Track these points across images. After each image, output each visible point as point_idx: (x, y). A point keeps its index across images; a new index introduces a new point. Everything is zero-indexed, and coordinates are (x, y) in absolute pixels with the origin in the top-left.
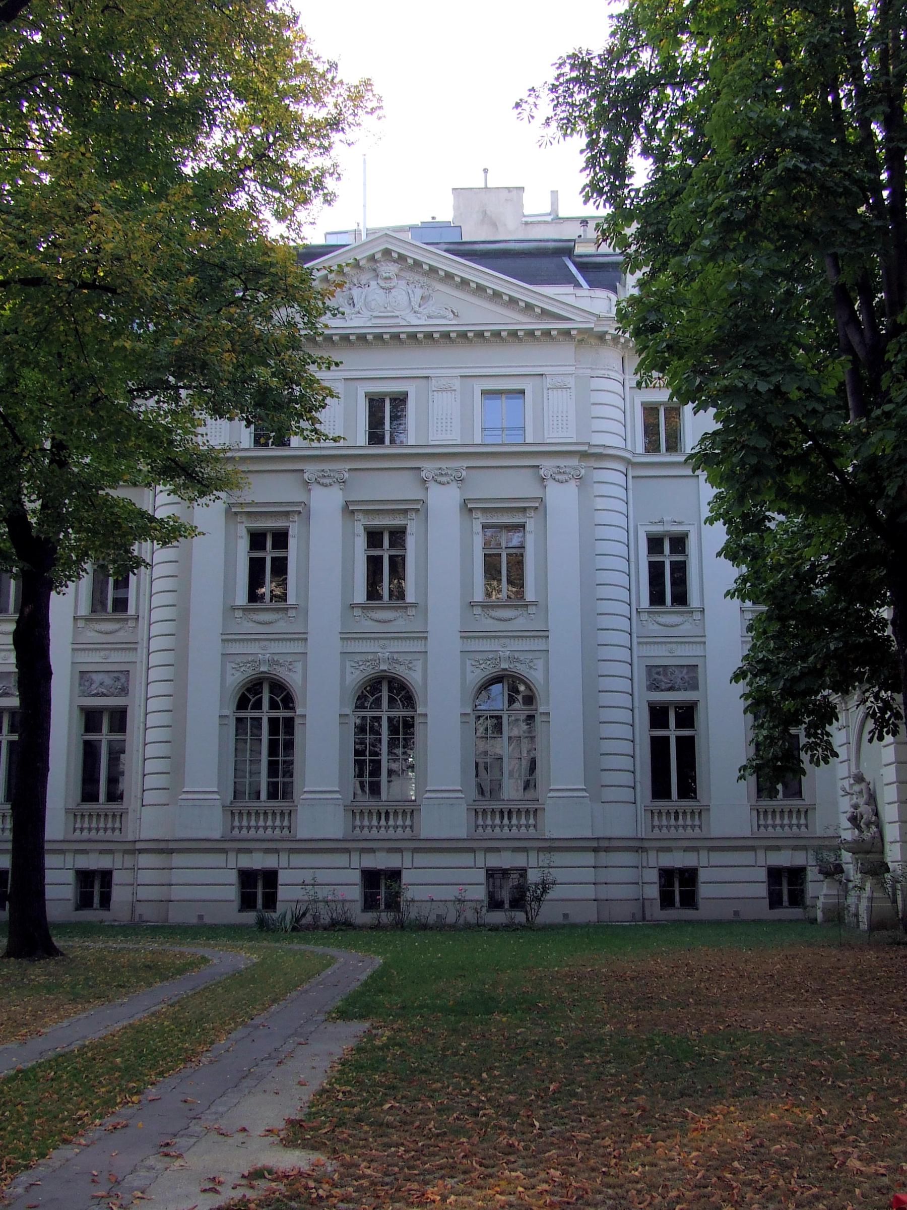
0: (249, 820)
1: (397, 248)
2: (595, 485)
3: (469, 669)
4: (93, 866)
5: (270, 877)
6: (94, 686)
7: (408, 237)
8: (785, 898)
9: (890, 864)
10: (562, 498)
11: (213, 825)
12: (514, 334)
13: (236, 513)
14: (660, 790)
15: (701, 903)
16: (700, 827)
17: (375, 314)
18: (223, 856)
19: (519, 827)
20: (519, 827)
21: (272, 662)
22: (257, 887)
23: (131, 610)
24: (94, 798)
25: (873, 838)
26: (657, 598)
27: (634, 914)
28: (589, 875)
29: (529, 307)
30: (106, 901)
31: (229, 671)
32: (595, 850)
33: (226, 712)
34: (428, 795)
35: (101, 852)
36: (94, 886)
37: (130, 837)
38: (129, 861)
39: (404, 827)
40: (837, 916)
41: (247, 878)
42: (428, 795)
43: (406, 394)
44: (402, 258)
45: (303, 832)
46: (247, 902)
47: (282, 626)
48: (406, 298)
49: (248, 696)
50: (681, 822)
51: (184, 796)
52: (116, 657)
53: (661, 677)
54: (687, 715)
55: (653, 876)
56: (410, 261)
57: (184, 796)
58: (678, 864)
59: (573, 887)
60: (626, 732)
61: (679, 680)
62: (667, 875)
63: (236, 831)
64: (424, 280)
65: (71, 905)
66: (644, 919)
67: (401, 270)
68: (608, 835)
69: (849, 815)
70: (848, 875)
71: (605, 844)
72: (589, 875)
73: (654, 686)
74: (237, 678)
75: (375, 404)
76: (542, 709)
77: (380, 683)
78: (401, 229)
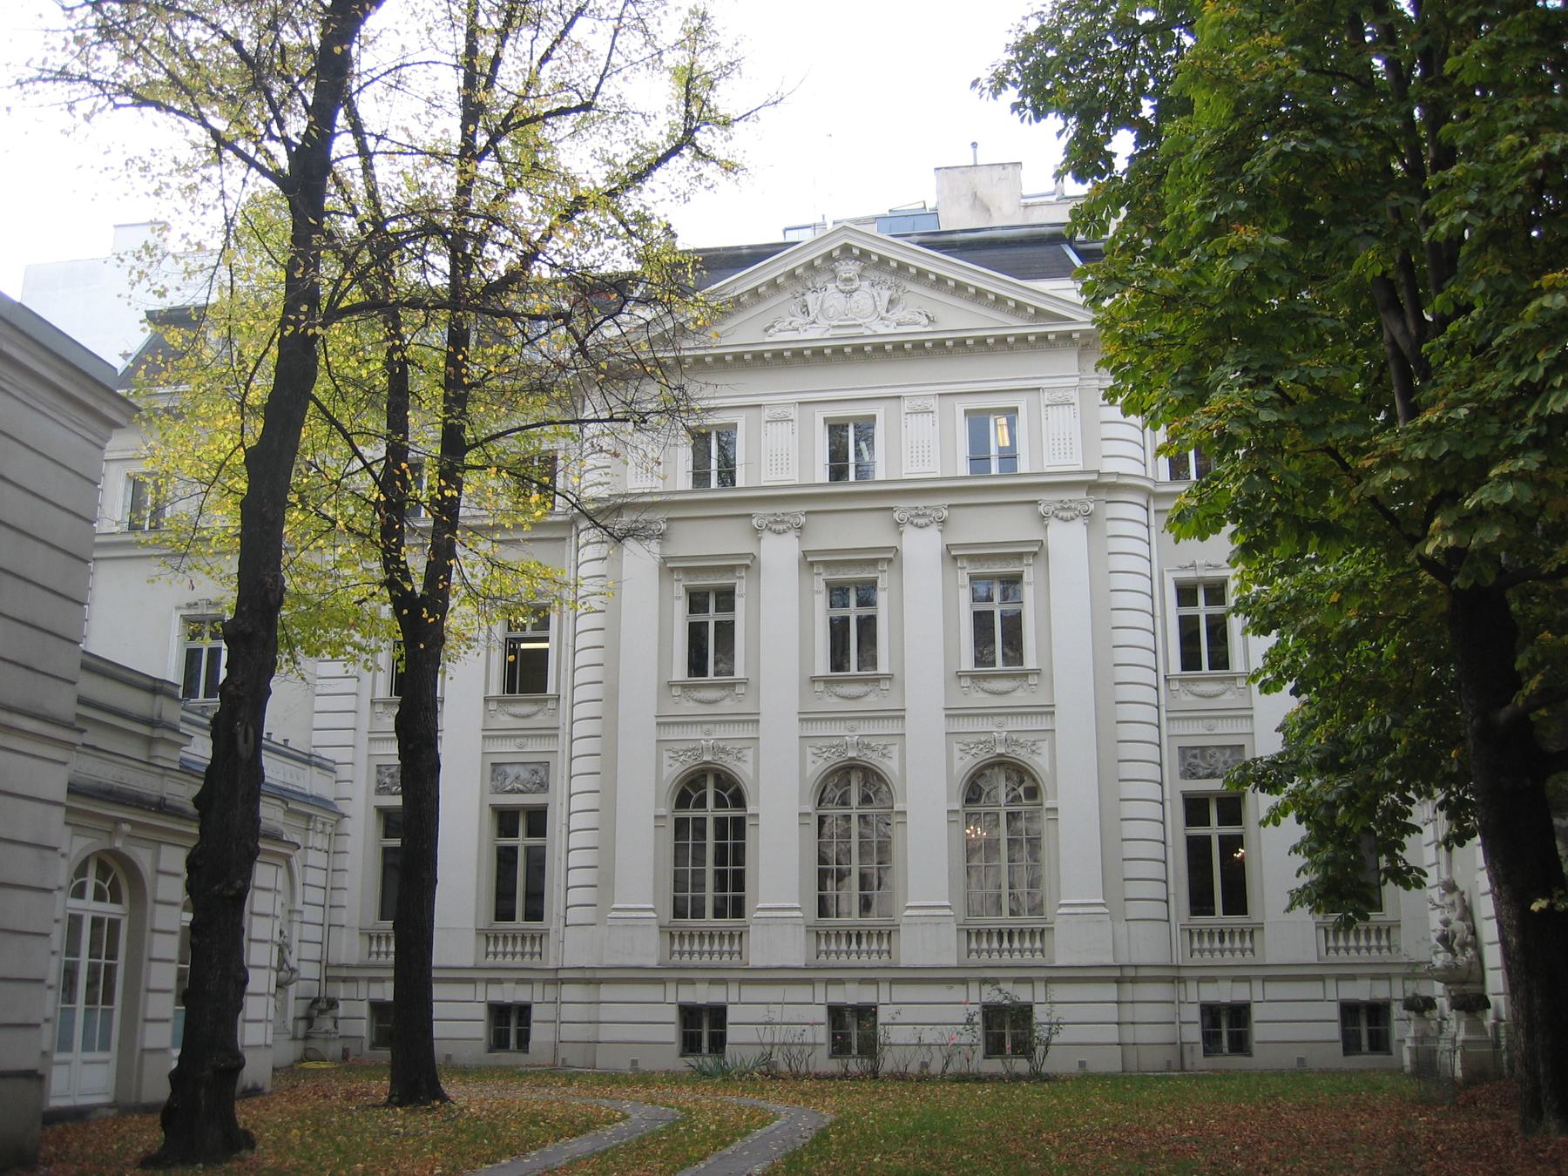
0: (505, 945)
1: (858, 243)
2: (1109, 523)
3: (957, 754)
4: (508, 1000)
5: (718, 1014)
6: (508, 781)
7: (872, 229)
8: (1365, 1041)
9: (1491, 998)
10: (1067, 541)
11: (647, 949)
12: (1001, 340)
13: (672, 569)
14: (1200, 902)
15: (1255, 1048)
16: (1252, 951)
17: (836, 323)
18: (809, 988)
19: (869, 953)
20: (869, 953)
21: (715, 750)
22: (702, 1027)
23: (551, 690)
24: (511, 917)
25: (1470, 963)
26: (1190, 660)
27: (1169, 1062)
28: (1111, 1012)
29: (1020, 307)
30: (524, 1041)
31: (666, 761)
32: (1119, 981)
33: (663, 811)
34: (908, 912)
35: (712, 982)
36: (509, 1023)
37: (552, 965)
38: (550, 992)
39: (879, 953)
40: (1426, 1065)
41: (690, 1015)
42: (908, 912)
43: (874, 417)
44: (864, 255)
45: (756, 959)
46: (690, 1045)
47: (728, 706)
48: (871, 302)
49: (688, 791)
50: (1227, 944)
51: (614, 914)
52: (533, 745)
53: (1198, 761)
54: (537, 820)
55: (1194, 1013)
56: (875, 258)
57: (614, 914)
58: (1226, 999)
59: (1081, 1029)
60: (1154, 830)
61: (1221, 765)
62: (1211, 1012)
63: (823, 957)
64: (890, 280)
65: (482, 1046)
66: (1183, 1069)
67: (864, 269)
68: (1135, 961)
69: (1438, 933)
70: (1441, 1012)
71: (1130, 973)
72: (1111, 1012)
73: (1190, 773)
74: (674, 770)
75: (836, 430)
76: (1048, 804)
77: (705, 776)
78: (857, 221)
